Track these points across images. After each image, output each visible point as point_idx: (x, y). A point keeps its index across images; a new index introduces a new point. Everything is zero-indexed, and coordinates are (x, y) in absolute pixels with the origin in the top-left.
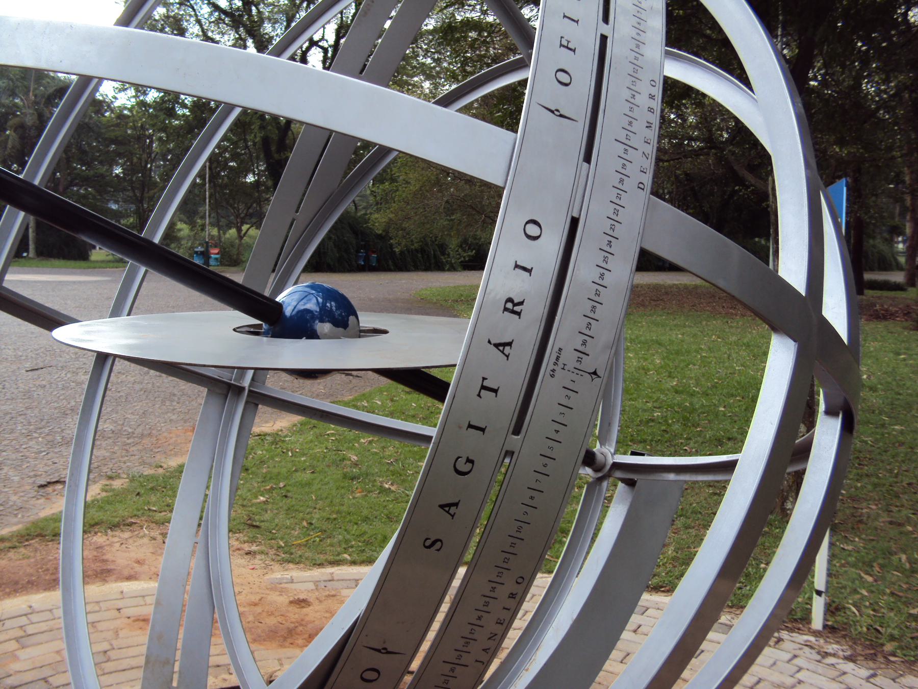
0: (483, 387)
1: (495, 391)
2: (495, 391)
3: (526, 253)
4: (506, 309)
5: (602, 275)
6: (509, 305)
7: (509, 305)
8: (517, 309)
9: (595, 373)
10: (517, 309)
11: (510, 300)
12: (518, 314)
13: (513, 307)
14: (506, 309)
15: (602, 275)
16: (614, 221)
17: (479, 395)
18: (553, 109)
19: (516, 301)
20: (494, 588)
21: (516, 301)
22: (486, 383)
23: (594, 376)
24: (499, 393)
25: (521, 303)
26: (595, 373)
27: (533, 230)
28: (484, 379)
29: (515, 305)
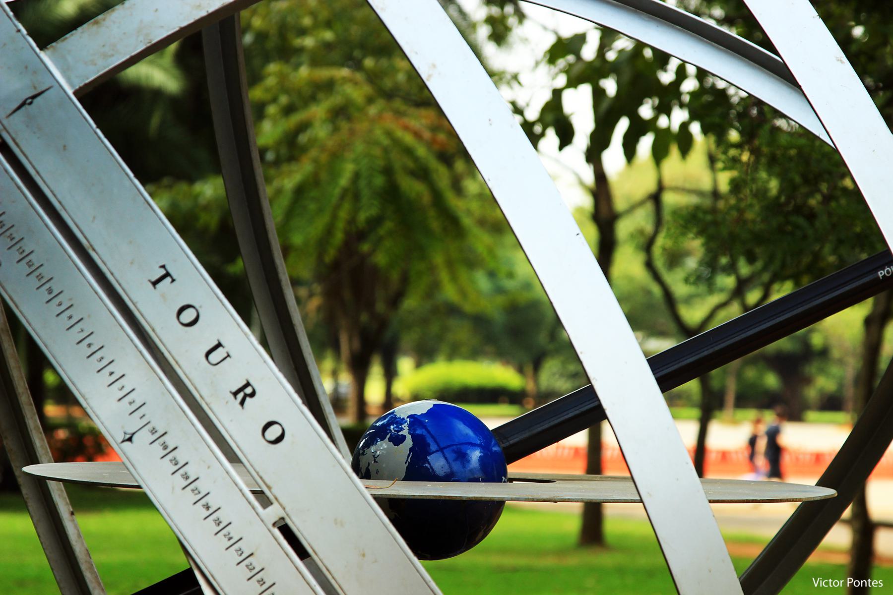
0: (168, 274)
1: (155, 283)
2: (155, 283)
3: (257, 410)
4: (248, 384)
5: (208, 508)
6: (248, 390)
7: (248, 390)
8: (240, 396)
9: (130, 439)
10: (240, 396)
11: (253, 395)
12: (235, 394)
13: (245, 393)
14: (248, 384)
15: (165, 448)
16: (234, 542)
17: (163, 267)
18: (36, 101)
19: (248, 399)
20: (165, 448)
21: (248, 399)
22: (169, 279)
23: (128, 436)
24: (151, 286)
25: (242, 403)
26: (130, 439)
27: (273, 432)
28: (173, 280)
29: (246, 396)
